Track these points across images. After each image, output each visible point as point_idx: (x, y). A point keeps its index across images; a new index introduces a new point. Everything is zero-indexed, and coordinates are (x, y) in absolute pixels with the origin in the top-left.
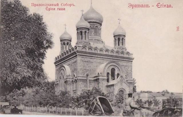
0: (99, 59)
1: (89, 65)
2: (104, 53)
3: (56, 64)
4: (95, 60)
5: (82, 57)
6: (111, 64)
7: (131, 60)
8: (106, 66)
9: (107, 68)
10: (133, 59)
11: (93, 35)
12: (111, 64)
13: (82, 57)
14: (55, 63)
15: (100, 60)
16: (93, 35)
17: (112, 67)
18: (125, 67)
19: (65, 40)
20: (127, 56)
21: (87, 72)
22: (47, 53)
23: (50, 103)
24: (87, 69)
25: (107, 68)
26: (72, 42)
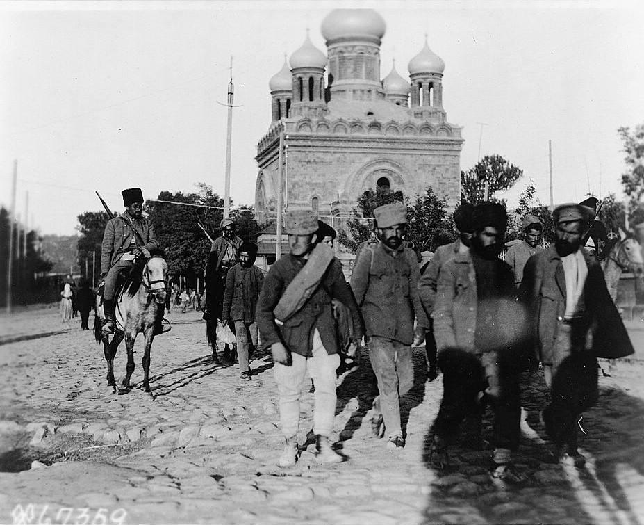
0: (351, 153)
1: (320, 172)
2: (365, 134)
3: (261, 163)
4: (337, 155)
5: (299, 151)
6: (377, 167)
7: (456, 148)
8: (360, 172)
9: (366, 173)
10: (460, 142)
11: (352, 75)
12: (372, 169)
13: (299, 151)
14: (258, 159)
15: (353, 155)
16: (352, 75)
17: (381, 175)
18: (434, 169)
19: (282, 91)
20: (443, 136)
21: (314, 189)
22: (117, 211)
23: (629, 183)
24: (314, 182)
25: (366, 173)
26: (381, 48)
